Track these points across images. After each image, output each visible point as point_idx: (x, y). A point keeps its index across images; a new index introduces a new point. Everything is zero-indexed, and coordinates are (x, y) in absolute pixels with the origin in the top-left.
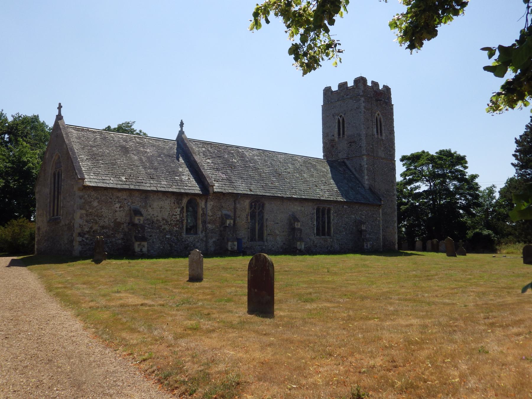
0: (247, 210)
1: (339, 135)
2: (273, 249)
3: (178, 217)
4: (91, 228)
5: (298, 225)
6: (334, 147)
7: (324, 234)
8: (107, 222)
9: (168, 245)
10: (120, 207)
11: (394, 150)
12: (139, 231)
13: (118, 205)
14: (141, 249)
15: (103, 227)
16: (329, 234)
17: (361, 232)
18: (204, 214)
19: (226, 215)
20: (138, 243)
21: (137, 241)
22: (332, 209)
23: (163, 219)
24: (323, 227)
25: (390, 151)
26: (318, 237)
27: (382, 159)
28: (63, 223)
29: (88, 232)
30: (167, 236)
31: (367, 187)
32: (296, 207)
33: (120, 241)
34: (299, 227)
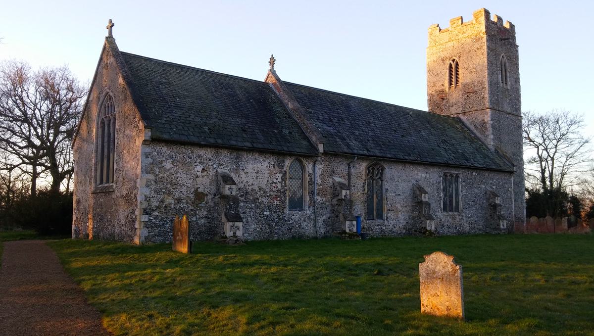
0: (364, 177)
1: (451, 84)
2: (394, 229)
3: (279, 185)
4: (162, 201)
5: (425, 198)
6: (443, 99)
7: (451, 211)
8: (185, 193)
9: (267, 226)
10: (203, 170)
11: (520, 102)
12: (230, 206)
13: (199, 168)
14: (235, 233)
15: (179, 200)
16: (457, 209)
17: (495, 207)
18: (312, 182)
19: (340, 183)
20: (231, 224)
21: (229, 221)
22: (461, 176)
23: (260, 189)
24: (451, 201)
25: (516, 105)
26: (445, 213)
27: (509, 114)
28: (117, 193)
29: (158, 207)
30: (265, 213)
31: (493, 150)
32: (419, 174)
33: (203, 221)
34: (427, 200)
